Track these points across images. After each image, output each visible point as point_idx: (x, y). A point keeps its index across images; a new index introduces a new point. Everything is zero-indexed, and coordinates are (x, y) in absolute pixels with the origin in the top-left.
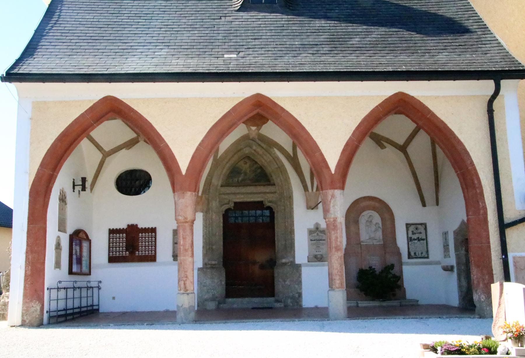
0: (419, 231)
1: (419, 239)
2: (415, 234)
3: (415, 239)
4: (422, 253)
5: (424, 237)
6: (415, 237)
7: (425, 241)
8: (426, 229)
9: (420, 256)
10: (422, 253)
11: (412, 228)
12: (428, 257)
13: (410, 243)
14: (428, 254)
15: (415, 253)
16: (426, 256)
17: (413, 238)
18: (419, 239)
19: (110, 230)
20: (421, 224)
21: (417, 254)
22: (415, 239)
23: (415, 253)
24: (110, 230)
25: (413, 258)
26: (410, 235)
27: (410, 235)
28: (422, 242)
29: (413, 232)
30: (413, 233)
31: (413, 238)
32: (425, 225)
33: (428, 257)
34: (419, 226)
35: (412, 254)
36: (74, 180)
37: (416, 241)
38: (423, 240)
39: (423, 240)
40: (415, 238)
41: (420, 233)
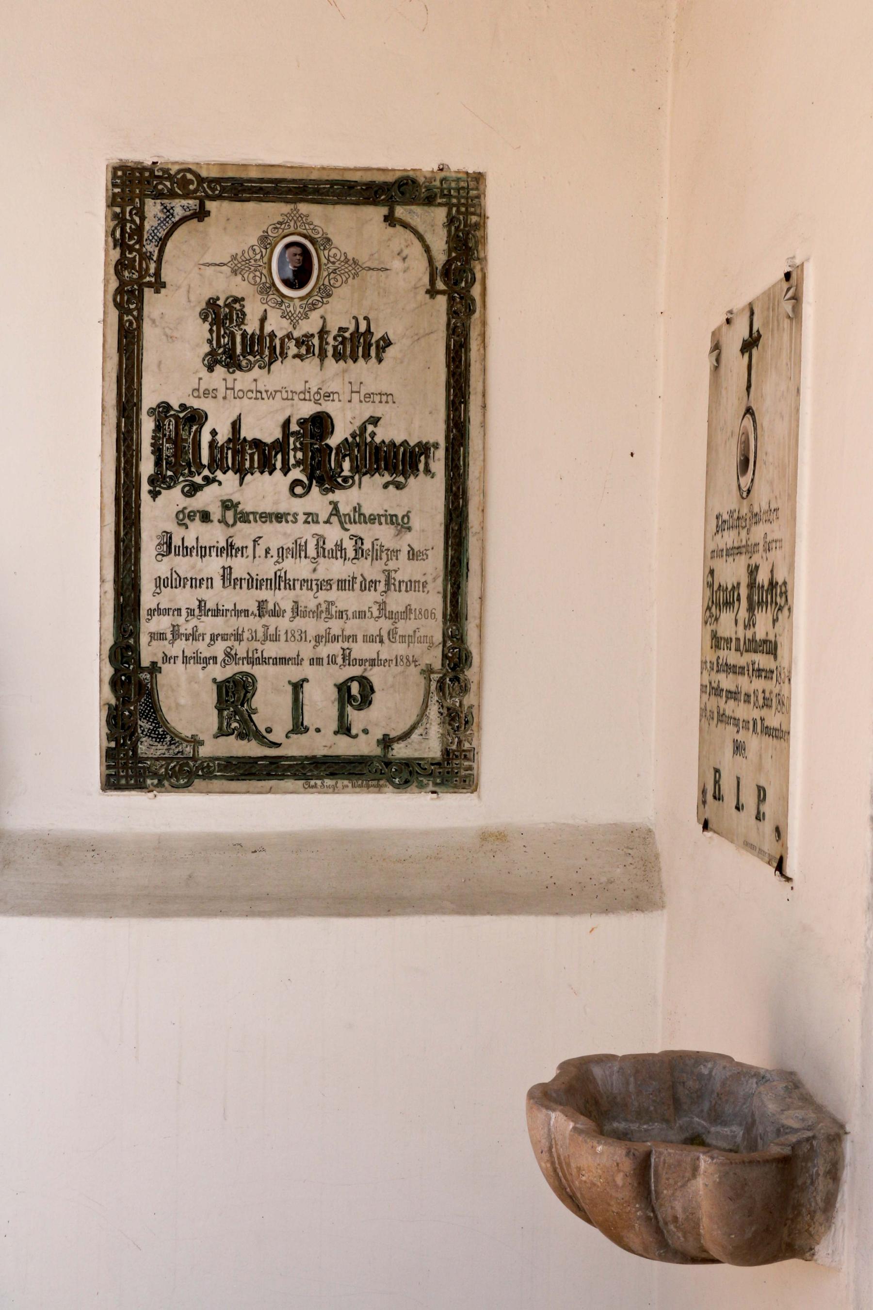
0: (339, 313)
1: (315, 453)
2: (263, 349)
3: (247, 455)
4: (355, 694)
5: (415, 419)
6: (260, 404)
7: (426, 494)
8: (458, 276)
9: (323, 742)
10: (355, 694)
11: (205, 260)
12: (452, 770)
13: (157, 513)
14: (459, 720)
15: (234, 695)
16: (429, 745)
17: (218, 423)
18: (315, 453)
19: (111, 783)
20: (391, 193)
21: (270, 706)
22: (247, 455)
23: (234, 695)
24: (111, 783)
25: (186, 771)
26: (176, 368)
27: (176, 368)
28: (370, 493)
29: (220, 314)
30: (234, 344)
31: (218, 423)
32: (448, 219)
33: (452, 770)
34: (350, 229)
35: (187, 701)
36: (738, 778)
37: (267, 490)
38: (400, 462)
39: (400, 462)
40: (263, 426)
41: (360, 344)
